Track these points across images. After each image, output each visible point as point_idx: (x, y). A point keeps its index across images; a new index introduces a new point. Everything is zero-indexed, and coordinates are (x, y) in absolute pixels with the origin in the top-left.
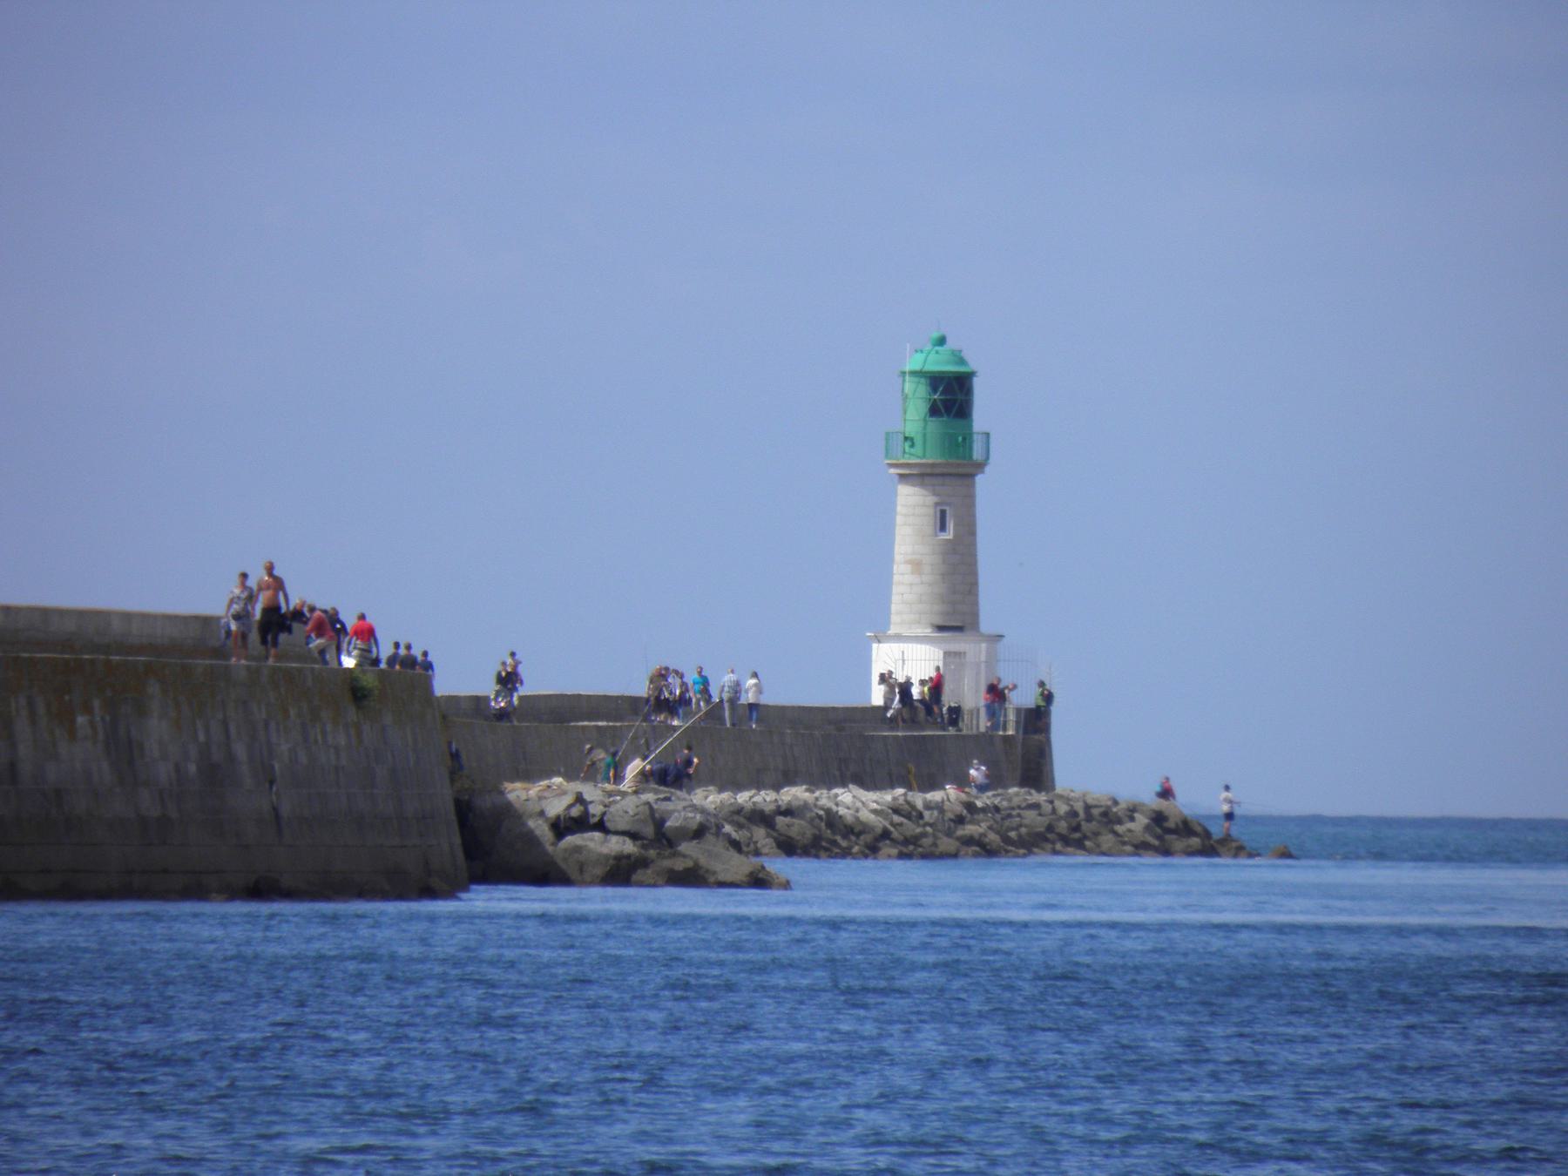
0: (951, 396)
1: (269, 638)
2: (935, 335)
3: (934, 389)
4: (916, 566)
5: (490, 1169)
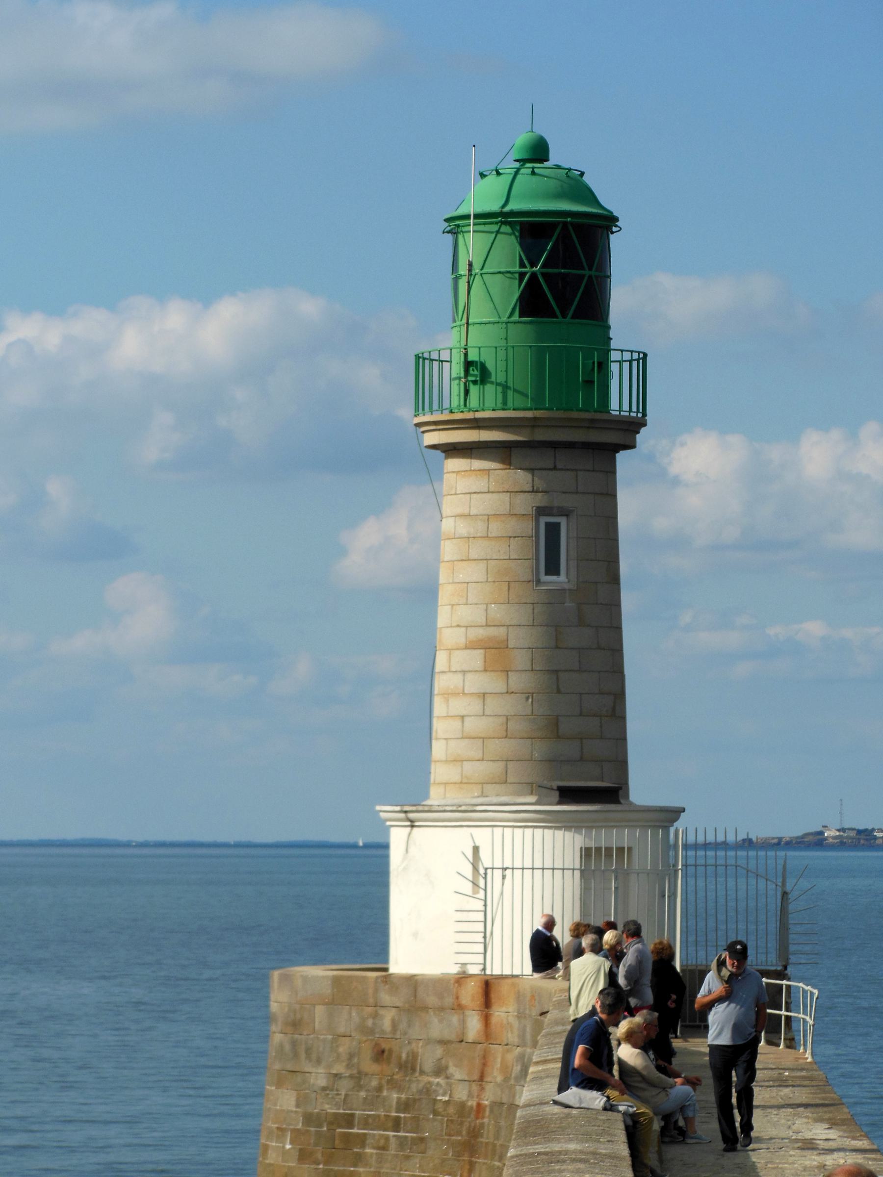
0: (562, 260)
1: (411, 1058)
2: (522, 139)
3: (530, 254)
4: (495, 652)
5: (164, 1175)
